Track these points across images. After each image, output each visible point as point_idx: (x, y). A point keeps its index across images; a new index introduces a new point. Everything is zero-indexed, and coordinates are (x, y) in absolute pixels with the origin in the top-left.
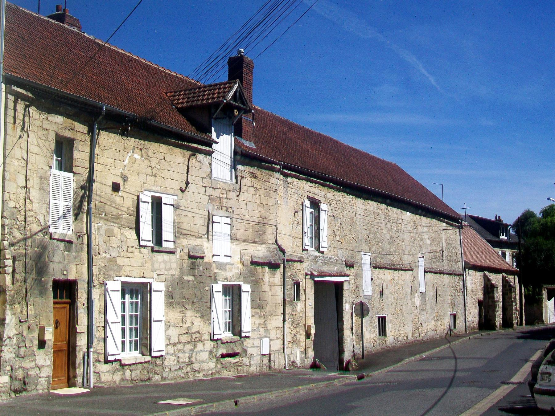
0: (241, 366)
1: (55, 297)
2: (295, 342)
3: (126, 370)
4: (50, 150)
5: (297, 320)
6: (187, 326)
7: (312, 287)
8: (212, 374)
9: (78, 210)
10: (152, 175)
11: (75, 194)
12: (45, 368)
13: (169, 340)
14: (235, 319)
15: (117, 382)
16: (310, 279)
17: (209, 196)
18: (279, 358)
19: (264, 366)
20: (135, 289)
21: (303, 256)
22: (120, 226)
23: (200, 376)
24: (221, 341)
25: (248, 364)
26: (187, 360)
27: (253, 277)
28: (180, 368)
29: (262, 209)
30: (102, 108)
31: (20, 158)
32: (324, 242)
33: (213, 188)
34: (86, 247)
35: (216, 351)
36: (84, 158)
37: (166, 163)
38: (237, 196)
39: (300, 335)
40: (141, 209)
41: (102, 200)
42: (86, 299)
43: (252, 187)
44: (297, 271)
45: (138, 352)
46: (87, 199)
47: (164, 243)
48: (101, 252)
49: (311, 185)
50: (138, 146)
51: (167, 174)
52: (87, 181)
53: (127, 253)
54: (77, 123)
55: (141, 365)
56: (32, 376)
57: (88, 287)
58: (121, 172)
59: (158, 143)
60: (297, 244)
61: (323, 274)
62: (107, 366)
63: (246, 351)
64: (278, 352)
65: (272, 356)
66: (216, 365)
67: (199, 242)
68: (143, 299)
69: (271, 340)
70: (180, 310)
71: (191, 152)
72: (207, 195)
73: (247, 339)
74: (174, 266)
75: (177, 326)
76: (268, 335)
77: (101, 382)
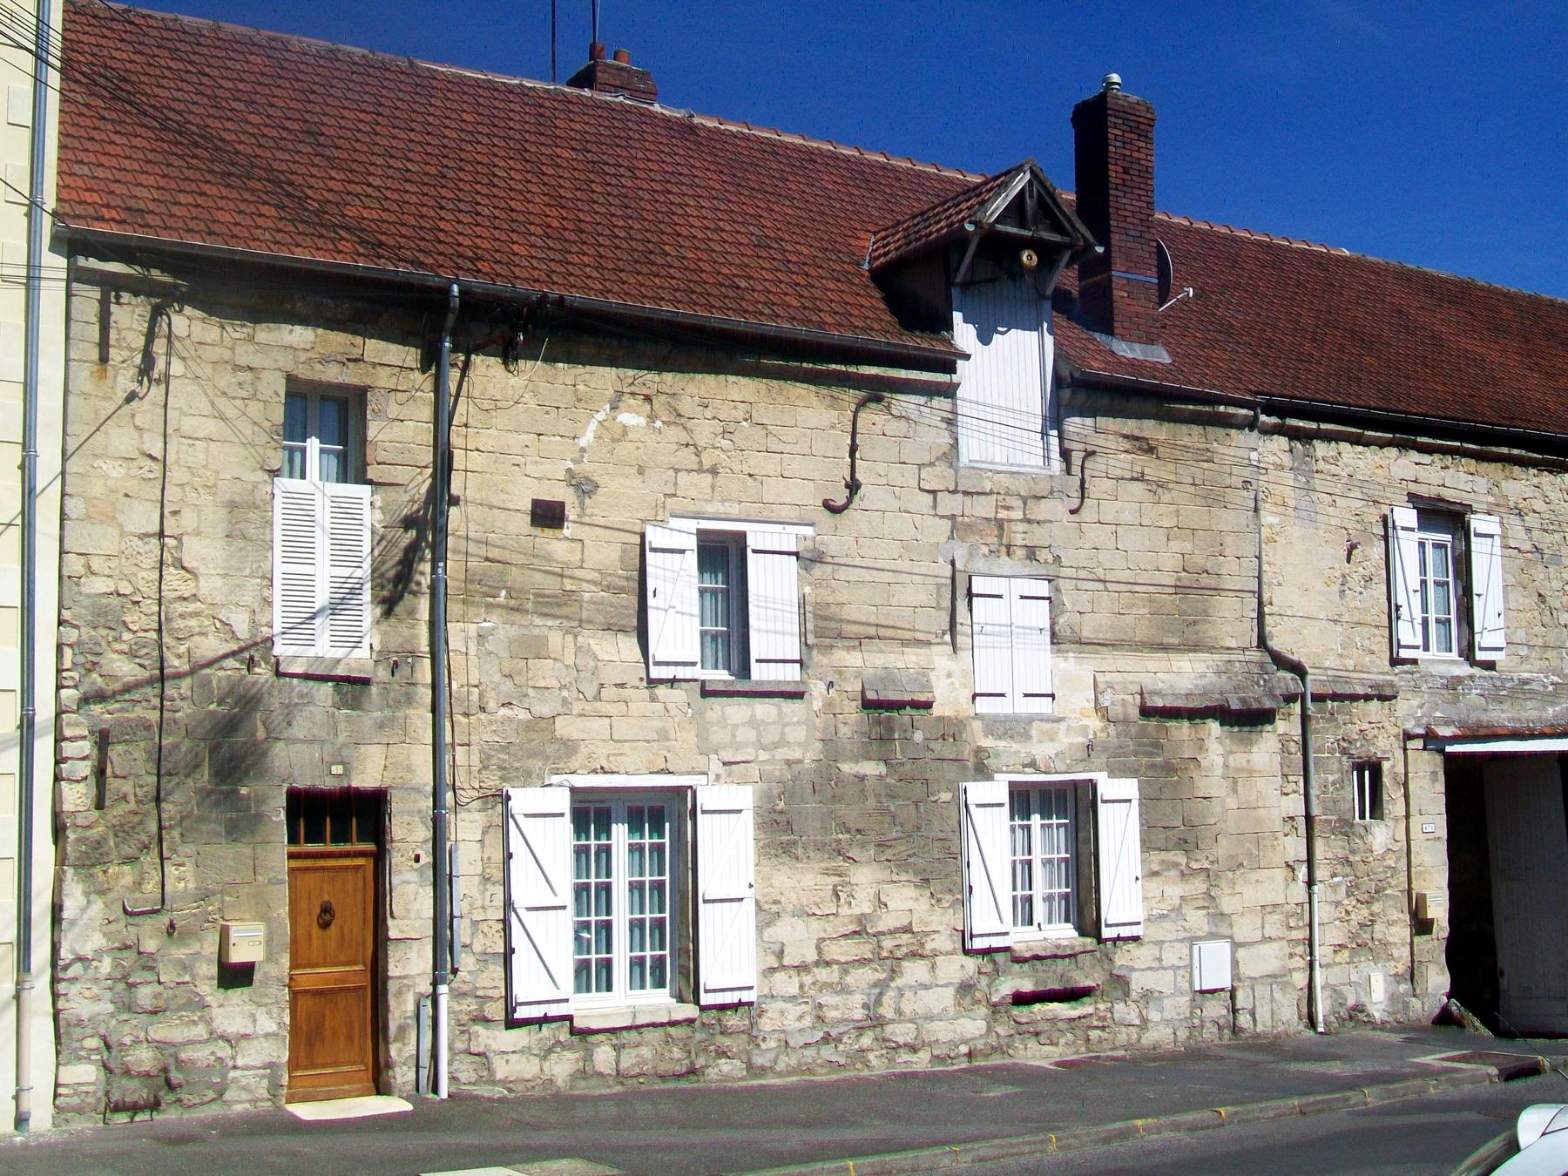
0: (1103, 1028)
1: (293, 839)
2: (1361, 945)
3: (598, 1045)
4: (266, 425)
5: (1372, 880)
6: (856, 911)
7: (1434, 773)
8: (970, 1055)
9: (396, 586)
10: (700, 471)
11: (379, 543)
12: (256, 1042)
13: (780, 954)
14: (1083, 883)
15: (560, 1082)
16: (1425, 749)
17: (953, 517)
18: (1272, 1000)
19: (1208, 1024)
20: (651, 809)
21: (1395, 679)
22: (575, 624)
23: (920, 1062)
24: (1008, 954)
25: (1137, 1022)
26: (859, 1014)
27: (1151, 754)
28: (826, 1039)
29: (1188, 547)
30: (448, 291)
31: (136, 454)
32: (1490, 630)
33: (966, 493)
34: (427, 695)
35: (989, 986)
36: (410, 440)
37: (759, 431)
38: (1072, 512)
39: (1389, 924)
40: (649, 570)
41: (494, 553)
42: (425, 841)
43: (1137, 479)
44: (1365, 726)
45: (667, 991)
46: (428, 554)
47: (754, 666)
48: (492, 705)
49: (1426, 459)
50: (633, 389)
51: (757, 462)
52: (427, 503)
53: (597, 705)
54: (374, 341)
55: (660, 1030)
56: (199, 1064)
57: (435, 807)
58: (569, 470)
59: (717, 373)
60: (1367, 643)
61: (1482, 732)
62: (519, 1037)
63: (1128, 984)
64: (1270, 980)
65: (1240, 995)
66: (989, 1029)
67: (914, 658)
68: (678, 835)
69: (1236, 945)
70: (823, 865)
71: (861, 394)
72: (943, 517)
73: (1131, 946)
74: (798, 734)
75: (814, 914)
76: (1224, 930)
77: (493, 1082)
